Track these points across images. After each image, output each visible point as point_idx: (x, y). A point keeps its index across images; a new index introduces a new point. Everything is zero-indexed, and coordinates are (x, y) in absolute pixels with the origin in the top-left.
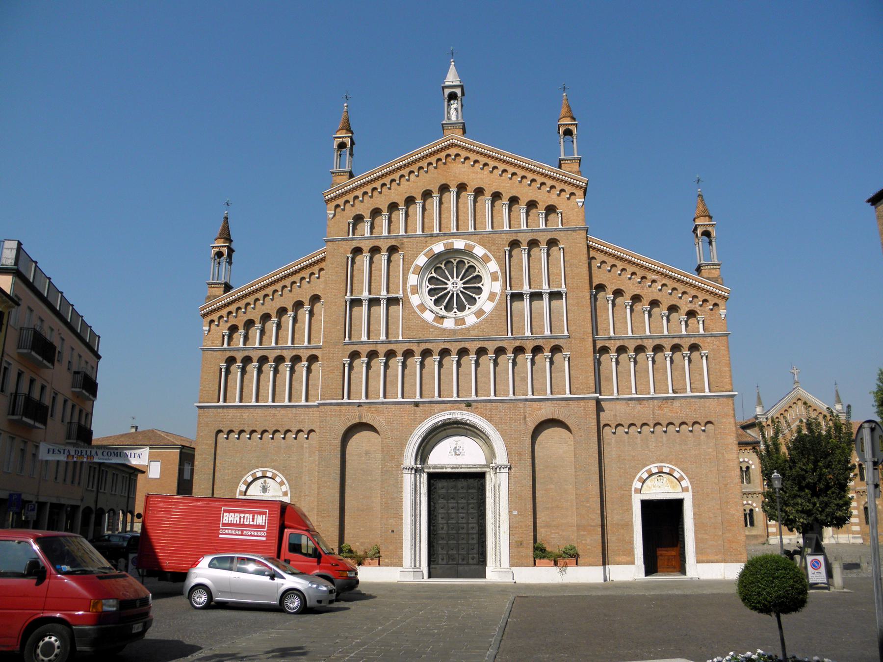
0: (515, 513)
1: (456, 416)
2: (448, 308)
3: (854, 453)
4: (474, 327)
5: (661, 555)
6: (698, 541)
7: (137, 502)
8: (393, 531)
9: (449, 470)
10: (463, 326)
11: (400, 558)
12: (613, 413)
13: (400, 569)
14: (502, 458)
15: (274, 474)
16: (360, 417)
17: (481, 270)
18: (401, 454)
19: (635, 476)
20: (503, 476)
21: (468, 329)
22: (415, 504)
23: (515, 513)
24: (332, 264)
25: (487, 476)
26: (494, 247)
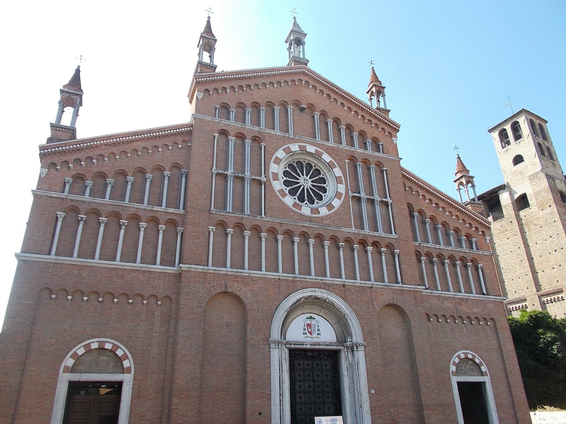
0: (373, 391)
4: (326, 217)
7: (511, 133)
8: (260, 414)
9: (309, 347)
10: (318, 215)
12: (429, 305)
14: (357, 336)
16: (226, 287)
17: (325, 173)
19: (450, 362)
20: (360, 355)
21: (322, 218)
24: (200, 138)
25: (343, 355)
26: (337, 158)
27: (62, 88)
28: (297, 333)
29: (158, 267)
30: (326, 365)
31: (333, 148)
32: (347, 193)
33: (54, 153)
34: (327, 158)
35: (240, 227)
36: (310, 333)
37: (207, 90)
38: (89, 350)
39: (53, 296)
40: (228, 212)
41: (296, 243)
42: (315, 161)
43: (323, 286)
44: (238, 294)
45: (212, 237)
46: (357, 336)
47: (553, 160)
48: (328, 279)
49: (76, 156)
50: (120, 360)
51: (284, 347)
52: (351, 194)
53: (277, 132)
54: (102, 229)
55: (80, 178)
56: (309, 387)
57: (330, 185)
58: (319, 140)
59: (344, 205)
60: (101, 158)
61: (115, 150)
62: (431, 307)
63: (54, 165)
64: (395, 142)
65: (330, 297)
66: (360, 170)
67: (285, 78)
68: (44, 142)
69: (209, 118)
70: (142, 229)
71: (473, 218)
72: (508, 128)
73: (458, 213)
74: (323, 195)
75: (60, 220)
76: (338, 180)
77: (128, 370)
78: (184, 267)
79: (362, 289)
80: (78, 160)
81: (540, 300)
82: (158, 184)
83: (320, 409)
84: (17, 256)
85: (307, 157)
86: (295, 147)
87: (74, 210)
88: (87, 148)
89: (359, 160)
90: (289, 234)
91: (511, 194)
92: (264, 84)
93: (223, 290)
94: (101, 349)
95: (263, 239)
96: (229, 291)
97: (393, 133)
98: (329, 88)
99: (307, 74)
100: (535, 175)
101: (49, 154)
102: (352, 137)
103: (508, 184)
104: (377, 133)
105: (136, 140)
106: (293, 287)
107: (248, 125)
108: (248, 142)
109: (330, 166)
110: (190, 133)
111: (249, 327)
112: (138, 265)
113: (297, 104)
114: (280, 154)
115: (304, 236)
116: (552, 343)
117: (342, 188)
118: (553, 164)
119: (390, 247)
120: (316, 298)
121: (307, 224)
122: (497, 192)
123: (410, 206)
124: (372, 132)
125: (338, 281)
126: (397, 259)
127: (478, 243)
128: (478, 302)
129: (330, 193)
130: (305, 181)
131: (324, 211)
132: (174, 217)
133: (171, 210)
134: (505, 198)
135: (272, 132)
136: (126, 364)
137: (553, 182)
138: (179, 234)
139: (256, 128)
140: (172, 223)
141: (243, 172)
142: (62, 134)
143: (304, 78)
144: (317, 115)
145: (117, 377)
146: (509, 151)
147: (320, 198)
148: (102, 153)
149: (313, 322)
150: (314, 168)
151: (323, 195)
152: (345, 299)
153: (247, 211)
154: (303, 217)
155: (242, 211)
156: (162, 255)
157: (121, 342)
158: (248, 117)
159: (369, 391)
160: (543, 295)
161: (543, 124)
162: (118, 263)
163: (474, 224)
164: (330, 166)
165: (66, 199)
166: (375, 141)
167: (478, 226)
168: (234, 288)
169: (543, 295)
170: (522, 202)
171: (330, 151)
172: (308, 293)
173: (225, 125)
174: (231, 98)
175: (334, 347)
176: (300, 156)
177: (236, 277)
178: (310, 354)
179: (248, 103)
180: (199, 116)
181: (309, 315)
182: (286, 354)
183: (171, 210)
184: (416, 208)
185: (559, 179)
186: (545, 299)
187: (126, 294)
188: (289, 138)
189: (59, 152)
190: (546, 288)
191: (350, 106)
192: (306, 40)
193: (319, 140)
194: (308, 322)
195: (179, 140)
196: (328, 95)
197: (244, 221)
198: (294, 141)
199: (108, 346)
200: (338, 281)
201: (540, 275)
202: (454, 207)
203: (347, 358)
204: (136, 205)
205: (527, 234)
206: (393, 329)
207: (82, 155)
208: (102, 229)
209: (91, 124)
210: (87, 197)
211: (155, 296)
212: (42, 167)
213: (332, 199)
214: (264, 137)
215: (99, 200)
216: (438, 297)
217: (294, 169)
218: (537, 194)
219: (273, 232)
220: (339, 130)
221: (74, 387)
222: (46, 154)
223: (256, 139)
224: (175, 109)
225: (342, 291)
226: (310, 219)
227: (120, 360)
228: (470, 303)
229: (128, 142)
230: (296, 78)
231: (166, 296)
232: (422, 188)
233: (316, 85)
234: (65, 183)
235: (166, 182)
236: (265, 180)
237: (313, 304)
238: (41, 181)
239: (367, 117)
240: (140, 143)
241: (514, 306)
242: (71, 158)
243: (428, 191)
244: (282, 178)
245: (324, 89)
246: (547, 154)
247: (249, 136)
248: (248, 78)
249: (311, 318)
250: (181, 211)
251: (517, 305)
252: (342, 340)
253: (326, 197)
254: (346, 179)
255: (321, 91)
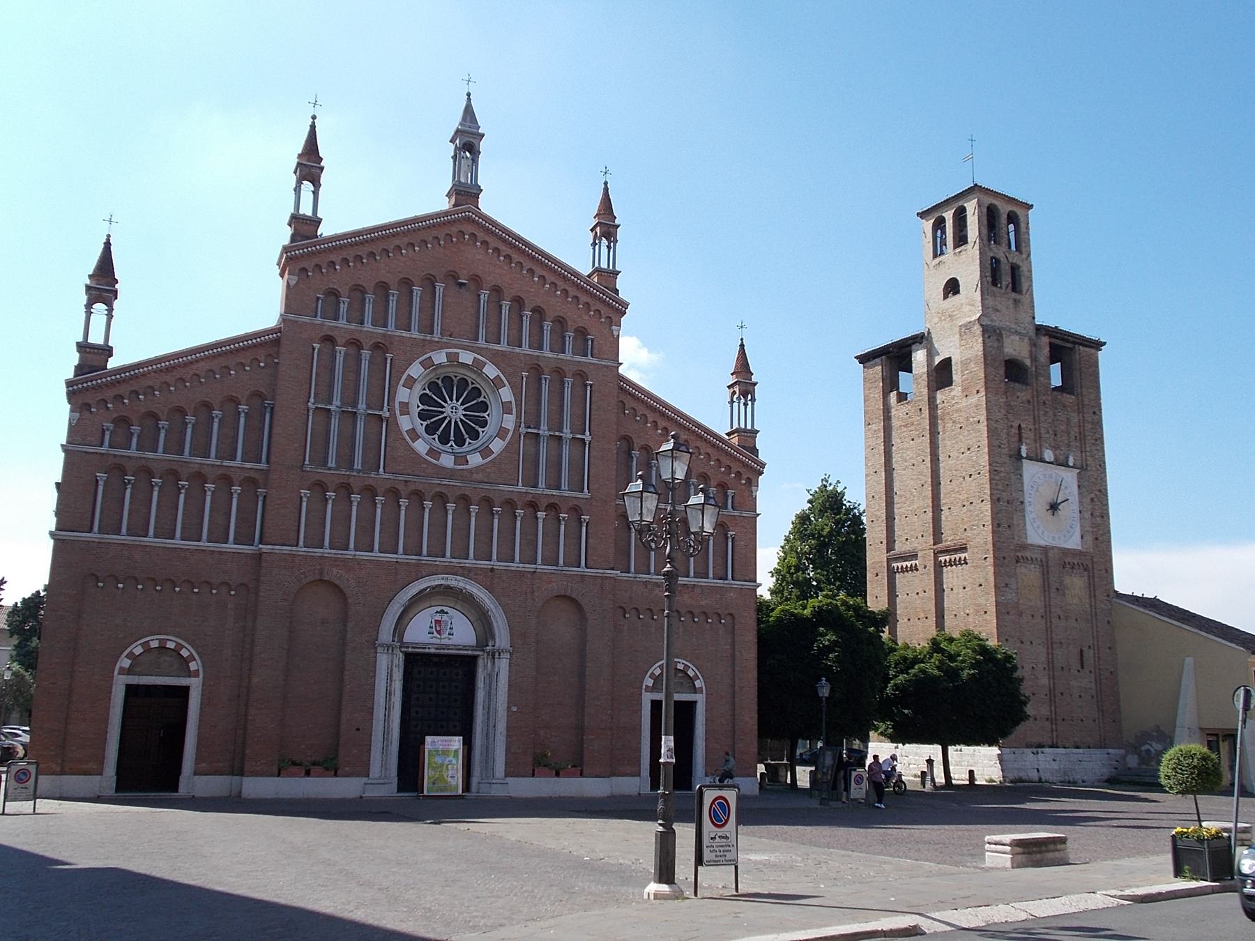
0: (514, 709)
1: (449, 583)
2: (430, 430)
3: (886, 629)
4: (478, 469)
5: (915, 776)
6: (105, 719)
9: (433, 651)
11: (367, 765)
13: (365, 780)
15: (178, 644)
16: (321, 573)
17: (487, 395)
18: (377, 629)
20: (503, 664)
21: (470, 471)
22: (389, 693)
23: (514, 709)
25: (480, 662)
27: (88, 282)
28: (419, 631)
29: (230, 547)
30: (457, 674)
31: (503, 354)
32: (517, 426)
33: (87, 389)
34: (491, 371)
35: (346, 489)
36: (439, 632)
37: (304, 270)
38: (147, 649)
39: (101, 584)
40: (330, 469)
41: (427, 510)
42: (474, 376)
43: (460, 571)
44: (337, 582)
45: (304, 504)
46: (502, 638)
47: (1020, 292)
48: (470, 562)
49: (115, 391)
50: (186, 662)
51: (397, 651)
52: (523, 430)
53: (414, 334)
54: (155, 494)
55: (123, 422)
56: (430, 699)
57: (493, 416)
58: (482, 343)
59: (511, 449)
60: (150, 390)
61: (168, 378)
62: (631, 598)
63: (87, 406)
64: (615, 333)
65: (467, 587)
66: (545, 387)
67: (435, 233)
68: (70, 374)
69: (306, 319)
70: (209, 493)
71: (735, 457)
72: (949, 215)
73: (710, 450)
74: (480, 430)
75: (101, 483)
76: (506, 408)
77: (196, 674)
78: (265, 548)
79: (521, 574)
80: (119, 398)
81: (936, 558)
82: (230, 424)
83: (442, 727)
84: (52, 534)
85: (462, 371)
86: (440, 357)
87: (118, 469)
88: (131, 378)
89: (546, 370)
90: (418, 496)
91: (931, 354)
92: (399, 248)
93: (318, 577)
94: (162, 648)
95: (379, 506)
96: (326, 578)
97: (615, 319)
98: (510, 243)
99: (474, 221)
100: (967, 326)
101: (80, 391)
102: (542, 327)
103: (929, 333)
104: (585, 320)
105: (197, 361)
106: (417, 572)
107: (368, 326)
108: (366, 353)
109: (497, 384)
110: (277, 342)
111: (350, 625)
112: (203, 544)
113: (453, 276)
114: (416, 370)
115: (441, 498)
116: (830, 649)
117: (509, 421)
118: (1016, 302)
119: (576, 511)
120: (448, 587)
121: (445, 482)
122: (910, 345)
123: (627, 439)
124: (577, 316)
125: (483, 564)
126: (584, 529)
127: (737, 498)
128: (712, 589)
129: (490, 429)
130: (454, 410)
131: (475, 460)
132: (253, 474)
133: (248, 465)
134: (919, 357)
135: (405, 334)
136: (193, 666)
137: (996, 345)
138: (261, 498)
139: (380, 330)
140: (251, 483)
141: (355, 404)
142: (93, 357)
143: (468, 229)
144: (484, 295)
145: (182, 682)
146: (942, 266)
147: (475, 435)
148: (151, 383)
149: (445, 617)
150: (471, 386)
151: (480, 430)
152: (490, 589)
153: (358, 465)
154: (442, 472)
155: (351, 466)
156: (236, 527)
157: (185, 640)
158: (369, 308)
159: (509, 708)
160: (941, 552)
161: (1019, 211)
162: (178, 542)
163: (736, 467)
164: (497, 384)
165: (108, 455)
166: (582, 333)
167: (742, 470)
168: (333, 574)
169: (941, 552)
170: (942, 374)
171: (496, 358)
172: (436, 581)
173: (331, 328)
174: (341, 279)
175: (470, 652)
176: (449, 369)
177: (336, 560)
178: (436, 659)
179: (369, 285)
180: (291, 317)
181: (439, 609)
182: (399, 659)
183: (248, 465)
184: (638, 442)
185: (1017, 333)
186: (942, 559)
187: (189, 581)
188: (431, 342)
189: (93, 388)
190: (949, 539)
191: (544, 273)
192: (483, 146)
193: (482, 343)
194: (438, 617)
195: (261, 353)
196: (508, 257)
197: (351, 480)
198: (439, 346)
199: (171, 645)
200: (483, 564)
201: (945, 515)
202: (706, 440)
203: (485, 666)
204: (199, 460)
205: (940, 437)
206: (562, 629)
207: (124, 390)
208: (155, 494)
209: (136, 340)
210: (133, 452)
211: (228, 584)
212: (72, 411)
213: (491, 439)
214: (391, 343)
215: (150, 455)
216: (645, 583)
217: (442, 387)
218: (965, 364)
219: (394, 494)
220: (522, 316)
221: (131, 690)
222: (75, 391)
223: (379, 348)
224: (253, 301)
225: (489, 579)
226: (450, 474)
227: (186, 662)
228: (698, 591)
229: (186, 365)
230: (454, 230)
231: (242, 584)
232: (654, 410)
233: (487, 239)
234: (103, 431)
235: (242, 420)
236: (387, 414)
237: (439, 593)
238: (73, 430)
239: (572, 291)
240: (202, 364)
241: (899, 565)
242: (109, 394)
243: (663, 414)
244: (416, 407)
245: (502, 247)
246: (1006, 280)
247: (367, 343)
248: (372, 240)
249: (442, 612)
250: (263, 466)
251: (904, 564)
252: (482, 644)
253: (485, 433)
254: (519, 405)
255: (496, 250)
